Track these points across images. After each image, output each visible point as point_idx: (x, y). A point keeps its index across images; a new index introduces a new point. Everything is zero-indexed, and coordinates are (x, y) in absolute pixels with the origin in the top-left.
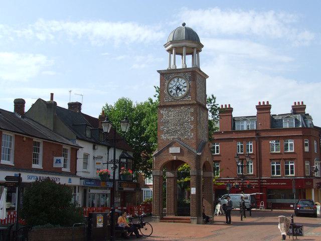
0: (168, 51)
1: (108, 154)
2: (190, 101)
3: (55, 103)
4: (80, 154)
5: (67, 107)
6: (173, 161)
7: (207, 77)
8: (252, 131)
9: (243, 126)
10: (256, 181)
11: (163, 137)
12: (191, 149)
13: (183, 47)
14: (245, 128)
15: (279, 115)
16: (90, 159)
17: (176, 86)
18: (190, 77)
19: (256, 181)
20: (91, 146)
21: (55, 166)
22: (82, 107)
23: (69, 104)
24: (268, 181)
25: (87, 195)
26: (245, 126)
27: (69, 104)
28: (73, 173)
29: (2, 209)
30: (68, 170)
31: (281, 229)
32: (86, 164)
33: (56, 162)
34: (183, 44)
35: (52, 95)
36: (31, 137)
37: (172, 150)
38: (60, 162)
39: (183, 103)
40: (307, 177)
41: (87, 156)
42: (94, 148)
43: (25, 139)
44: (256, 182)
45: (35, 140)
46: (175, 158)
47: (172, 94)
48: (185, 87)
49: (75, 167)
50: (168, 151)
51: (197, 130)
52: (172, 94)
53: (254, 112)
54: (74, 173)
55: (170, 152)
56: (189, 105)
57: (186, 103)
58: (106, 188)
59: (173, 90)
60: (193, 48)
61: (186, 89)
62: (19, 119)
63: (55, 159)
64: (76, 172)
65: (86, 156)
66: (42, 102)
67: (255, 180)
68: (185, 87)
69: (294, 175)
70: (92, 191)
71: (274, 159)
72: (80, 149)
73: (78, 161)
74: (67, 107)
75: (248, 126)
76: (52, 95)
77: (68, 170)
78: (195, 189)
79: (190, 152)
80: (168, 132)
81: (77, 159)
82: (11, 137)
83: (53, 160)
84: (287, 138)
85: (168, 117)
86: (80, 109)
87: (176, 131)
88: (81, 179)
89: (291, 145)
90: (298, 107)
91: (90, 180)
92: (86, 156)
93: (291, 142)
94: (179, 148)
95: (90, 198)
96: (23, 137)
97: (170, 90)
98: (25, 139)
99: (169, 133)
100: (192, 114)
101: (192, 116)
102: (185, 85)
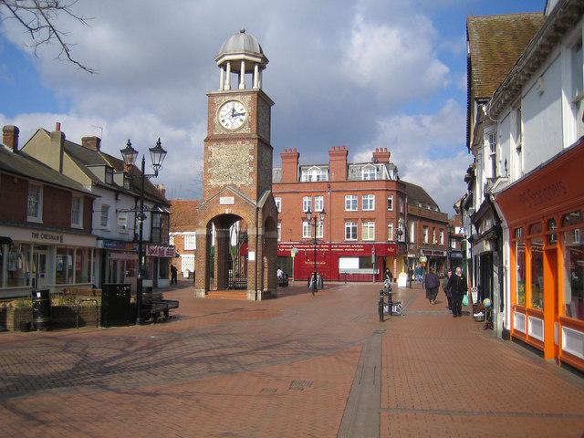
0: (220, 66)
4: (97, 206)
5: (80, 143)
6: (225, 215)
7: (273, 103)
13: (240, 60)
14: (314, 179)
15: (150, 323)
16: (111, 212)
22: (102, 143)
23: (83, 139)
25: (107, 262)
27: (83, 139)
28: (87, 230)
31: (226, 203)
32: (105, 219)
34: (242, 57)
35: (59, 125)
37: (224, 200)
42: (117, 199)
43: (16, 181)
45: (31, 182)
46: (227, 211)
58: (133, 252)
64: (92, 230)
70: (114, 256)
74: (80, 143)
75: (318, 177)
76: (59, 125)
77: (80, 226)
79: (247, 204)
82: (38, 187)
84: (366, 192)
87: (229, 176)
88: (98, 238)
89: (349, 207)
91: (111, 241)
92: (105, 209)
93: (371, 198)
96: (13, 178)
98: (16, 181)
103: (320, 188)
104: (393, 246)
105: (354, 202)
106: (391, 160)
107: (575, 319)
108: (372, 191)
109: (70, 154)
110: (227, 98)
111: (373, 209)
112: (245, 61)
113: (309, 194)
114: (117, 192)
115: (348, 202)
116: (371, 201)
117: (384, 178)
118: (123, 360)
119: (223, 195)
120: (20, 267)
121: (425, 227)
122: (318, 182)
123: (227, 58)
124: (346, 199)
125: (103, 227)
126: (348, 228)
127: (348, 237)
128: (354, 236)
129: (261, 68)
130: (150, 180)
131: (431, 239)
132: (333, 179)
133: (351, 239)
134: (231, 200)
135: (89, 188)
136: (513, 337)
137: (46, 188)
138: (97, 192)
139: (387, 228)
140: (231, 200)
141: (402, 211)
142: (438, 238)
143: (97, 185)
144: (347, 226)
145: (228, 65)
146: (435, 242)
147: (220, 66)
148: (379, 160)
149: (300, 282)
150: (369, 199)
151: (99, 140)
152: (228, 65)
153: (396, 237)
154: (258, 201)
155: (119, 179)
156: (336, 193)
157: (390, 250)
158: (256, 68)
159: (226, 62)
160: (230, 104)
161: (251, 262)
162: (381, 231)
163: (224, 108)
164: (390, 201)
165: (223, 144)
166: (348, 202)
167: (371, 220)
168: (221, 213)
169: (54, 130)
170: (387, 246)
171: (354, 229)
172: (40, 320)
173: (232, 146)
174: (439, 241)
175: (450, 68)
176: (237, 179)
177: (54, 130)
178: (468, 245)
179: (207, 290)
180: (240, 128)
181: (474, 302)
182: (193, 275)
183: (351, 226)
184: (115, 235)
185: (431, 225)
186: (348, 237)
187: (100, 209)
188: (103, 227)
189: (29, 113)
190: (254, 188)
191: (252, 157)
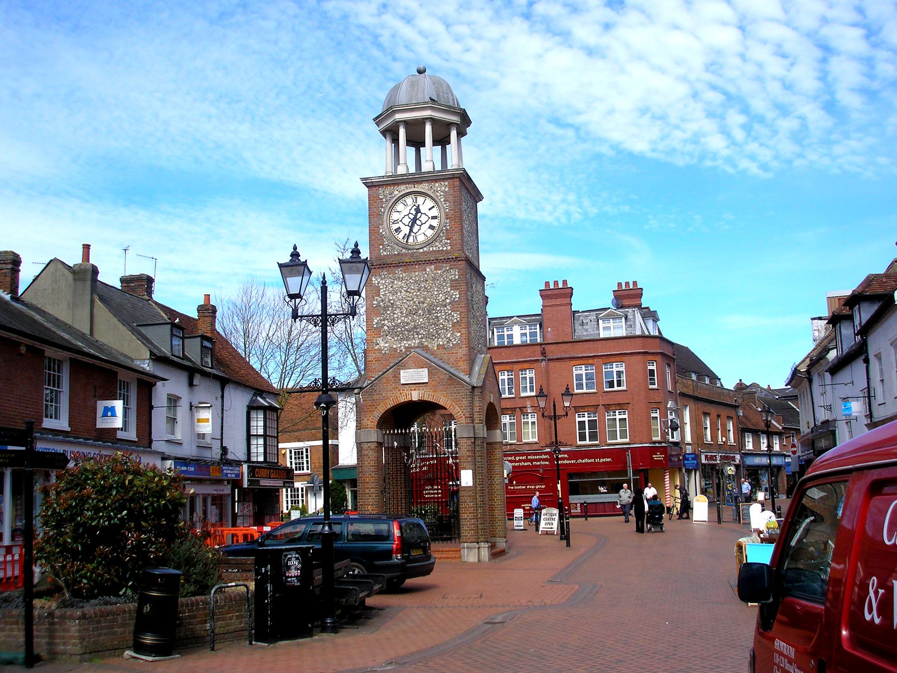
1: (222, 397)
3: (95, 271)
4: (161, 394)
5: (118, 285)
8: (533, 345)
9: (510, 337)
10: (543, 457)
12: (456, 373)
14: (517, 341)
18: (445, 192)
19: (543, 457)
20: (183, 377)
21: (101, 424)
22: (156, 287)
23: (123, 280)
24: (573, 455)
26: (517, 335)
30: (132, 435)
33: (105, 415)
34: (427, 113)
35: (87, 248)
36: (38, 345)
37: (407, 376)
38: (114, 415)
40: (655, 442)
41: (175, 401)
42: (191, 384)
43: (23, 350)
44: (287, 492)
45: (50, 352)
46: (415, 396)
47: (401, 236)
48: (434, 218)
49: (148, 427)
50: (397, 377)
51: (468, 326)
52: (401, 236)
53: (535, 306)
54: (146, 443)
55: (403, 381)
58: (219, 482)
61: (435, 223)
62: (6, 303)
63: (101, 405)
64: (151, 441)
65: (173, 401)
66: (60, 266)
67: (541, 454)
68: (434, 218)
71: (583, 407)
72: (159, 384)
74: (118, 285)
76: (87, 248)
77: (132, 435)
78: (470, 472)
79: (453, 379)
80: (392, 331)
81: (151, 407)
83: (94, 410)
85: (394, 293)
86: (150, 291)
88: (164, 458)
90: (626, 293)
92: (173, 401)
94: (426, 370)
96: (19, 344)
97: (395, 227)
102: (434, 212)
103: (528, 355)
104: (663, 450)
105: (589, 377)
106: (645, 302)
108: (619, 357)
109: (102, 299)
110: (404, 189)
111: (623, 388)
112: (433, 120)
113: (509, 366)
114: (192, 372)
115: (579, 377)
116: (531, 379)
117: (638, 333)
119: (405, 367)
121: (706, 414)
122: (523, 345)
123: (399, 116)
124: (575, 372)
126: (582, 423)
127: (583, 438)
129: (461, 134)
131: (714, 437)
132: (550, 339)
133: (587, 442)
134: (422, 375)
135: (147, 366)
137: (74, 363)
138: (159, 371)
139: (650, 420)
140: (422, 375)
141: (670, 388)
142: (725, 432)
143: (158, 359)
144: (578, 419)
145: (402, 132)
148: (626, 302)
149: (796, 539)
150: (528, 376)
151: (150, 281)
152: (402, 132)
153: (664, 434)
154: (470, 375)
155: (193, 350)
156: (557, 364)
157: (658, 457)
158: (454, 134)
159: (397, 124)
160: (409, 200)
162: (642, 425)
163: (400, 207)
164: (652, 372)
165: (399, 272)
166: (579, 377)
167: (621, 406)
168: (403, 399)
169: (79, 260)
170: (653, 450)
171: (592, 423)
173: (417, 274)
174: (728, 438)
176: (429, 336)
177: (79, 260)
180: (429, 242)
183: (586, 419)
184: (188, 450)
185: (712, 410)
186: (583, 438)
187: (165, 403)
188: (171, 437)
190: (463, 351)
191: (456, 295)
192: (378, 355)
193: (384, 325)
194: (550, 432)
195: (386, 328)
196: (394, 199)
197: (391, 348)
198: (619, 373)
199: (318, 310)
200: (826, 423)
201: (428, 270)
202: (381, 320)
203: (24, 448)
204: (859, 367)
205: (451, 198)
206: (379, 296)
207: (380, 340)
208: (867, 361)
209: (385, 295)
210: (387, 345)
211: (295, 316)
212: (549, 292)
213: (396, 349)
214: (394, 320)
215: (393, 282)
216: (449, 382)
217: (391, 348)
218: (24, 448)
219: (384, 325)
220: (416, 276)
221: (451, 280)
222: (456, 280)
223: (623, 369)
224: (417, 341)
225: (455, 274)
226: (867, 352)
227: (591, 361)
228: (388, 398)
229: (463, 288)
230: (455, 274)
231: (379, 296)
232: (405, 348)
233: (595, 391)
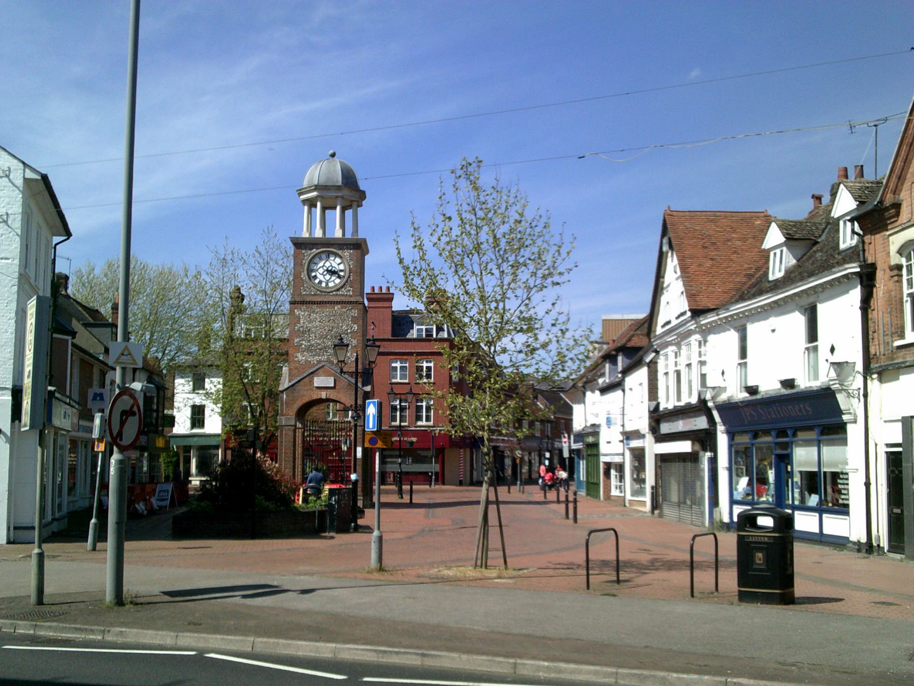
2: (351, 296)
11: (300, 357)
17: (325, 268)
29: (641, 384)
33: (94, 399)
35: (509, 492)
37: (318, 381)
38: (102, 399)
39: (338, 299)
47: (317, 281)
50: (312, 382)
55: (316, 385)
56: (350, 303)
57: (344, 299)
59: (318, 275)
60: (352, 201)
69: (431, 423)
73: (726, 465)
76: (509, 492)
80: (309, 349)
85: (311, 321)
94: (333, 378)
95: (666, 374)
97: (313, 274)
99: (311, 351)
100: (354, 320)
101: (355, 324)
107: (488, 381)
116: (428, 409)
118: (888, 363)
120: (675, 337)
125: (124, 366)
128: (419, 369)
130: (628, 346)
136: (643, 436)
138: (113, 365)
146: (779, 417)
147: (304, 202)
161: (359, 446)
172: (133, 498)
175: (866, 542)
178: (35, 623)
179: (69, 461)
181: (441, 455)
182: (653, 352)
189: (767, 604)
191: (356, 327)
192: (297, 365)
193: (302, 344)
194: (48, 337)
195: (303, 346)
196: (313, 255)
197: (306, 361)
198: (429, 368)
199: (353, 370)
200: (593, 425)
201: (336, 308)
202: (300, 341)
203: (377, 454)
204: (619, 393)
205: (355, 258)
206: (299, 323)
207: (299, 355)
208: (624, 391)
209: (304, 323)
210: (304, 358)
211: (342, 372)
212: (374, 296)
213: (310, 362)
214: (309, 341)
215: (310, 315)
216: (349, 387)
217: (306, 361)
218: (377, 454)
219: (302, 344)
220: (327, 312)
221: (352, 316)
222: (355, 317)
223: (432, 365)
224: (326, 357)
225: (355, 313)
226: (624, 385)
227: (405, 357)
228: (304, 396)
229: (361, 323)
230: (355, 313)
231: (299, 323)
232: (317, 361)
233: (407, 381)
